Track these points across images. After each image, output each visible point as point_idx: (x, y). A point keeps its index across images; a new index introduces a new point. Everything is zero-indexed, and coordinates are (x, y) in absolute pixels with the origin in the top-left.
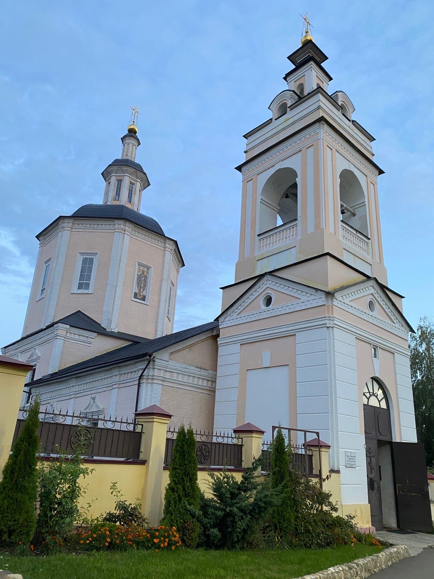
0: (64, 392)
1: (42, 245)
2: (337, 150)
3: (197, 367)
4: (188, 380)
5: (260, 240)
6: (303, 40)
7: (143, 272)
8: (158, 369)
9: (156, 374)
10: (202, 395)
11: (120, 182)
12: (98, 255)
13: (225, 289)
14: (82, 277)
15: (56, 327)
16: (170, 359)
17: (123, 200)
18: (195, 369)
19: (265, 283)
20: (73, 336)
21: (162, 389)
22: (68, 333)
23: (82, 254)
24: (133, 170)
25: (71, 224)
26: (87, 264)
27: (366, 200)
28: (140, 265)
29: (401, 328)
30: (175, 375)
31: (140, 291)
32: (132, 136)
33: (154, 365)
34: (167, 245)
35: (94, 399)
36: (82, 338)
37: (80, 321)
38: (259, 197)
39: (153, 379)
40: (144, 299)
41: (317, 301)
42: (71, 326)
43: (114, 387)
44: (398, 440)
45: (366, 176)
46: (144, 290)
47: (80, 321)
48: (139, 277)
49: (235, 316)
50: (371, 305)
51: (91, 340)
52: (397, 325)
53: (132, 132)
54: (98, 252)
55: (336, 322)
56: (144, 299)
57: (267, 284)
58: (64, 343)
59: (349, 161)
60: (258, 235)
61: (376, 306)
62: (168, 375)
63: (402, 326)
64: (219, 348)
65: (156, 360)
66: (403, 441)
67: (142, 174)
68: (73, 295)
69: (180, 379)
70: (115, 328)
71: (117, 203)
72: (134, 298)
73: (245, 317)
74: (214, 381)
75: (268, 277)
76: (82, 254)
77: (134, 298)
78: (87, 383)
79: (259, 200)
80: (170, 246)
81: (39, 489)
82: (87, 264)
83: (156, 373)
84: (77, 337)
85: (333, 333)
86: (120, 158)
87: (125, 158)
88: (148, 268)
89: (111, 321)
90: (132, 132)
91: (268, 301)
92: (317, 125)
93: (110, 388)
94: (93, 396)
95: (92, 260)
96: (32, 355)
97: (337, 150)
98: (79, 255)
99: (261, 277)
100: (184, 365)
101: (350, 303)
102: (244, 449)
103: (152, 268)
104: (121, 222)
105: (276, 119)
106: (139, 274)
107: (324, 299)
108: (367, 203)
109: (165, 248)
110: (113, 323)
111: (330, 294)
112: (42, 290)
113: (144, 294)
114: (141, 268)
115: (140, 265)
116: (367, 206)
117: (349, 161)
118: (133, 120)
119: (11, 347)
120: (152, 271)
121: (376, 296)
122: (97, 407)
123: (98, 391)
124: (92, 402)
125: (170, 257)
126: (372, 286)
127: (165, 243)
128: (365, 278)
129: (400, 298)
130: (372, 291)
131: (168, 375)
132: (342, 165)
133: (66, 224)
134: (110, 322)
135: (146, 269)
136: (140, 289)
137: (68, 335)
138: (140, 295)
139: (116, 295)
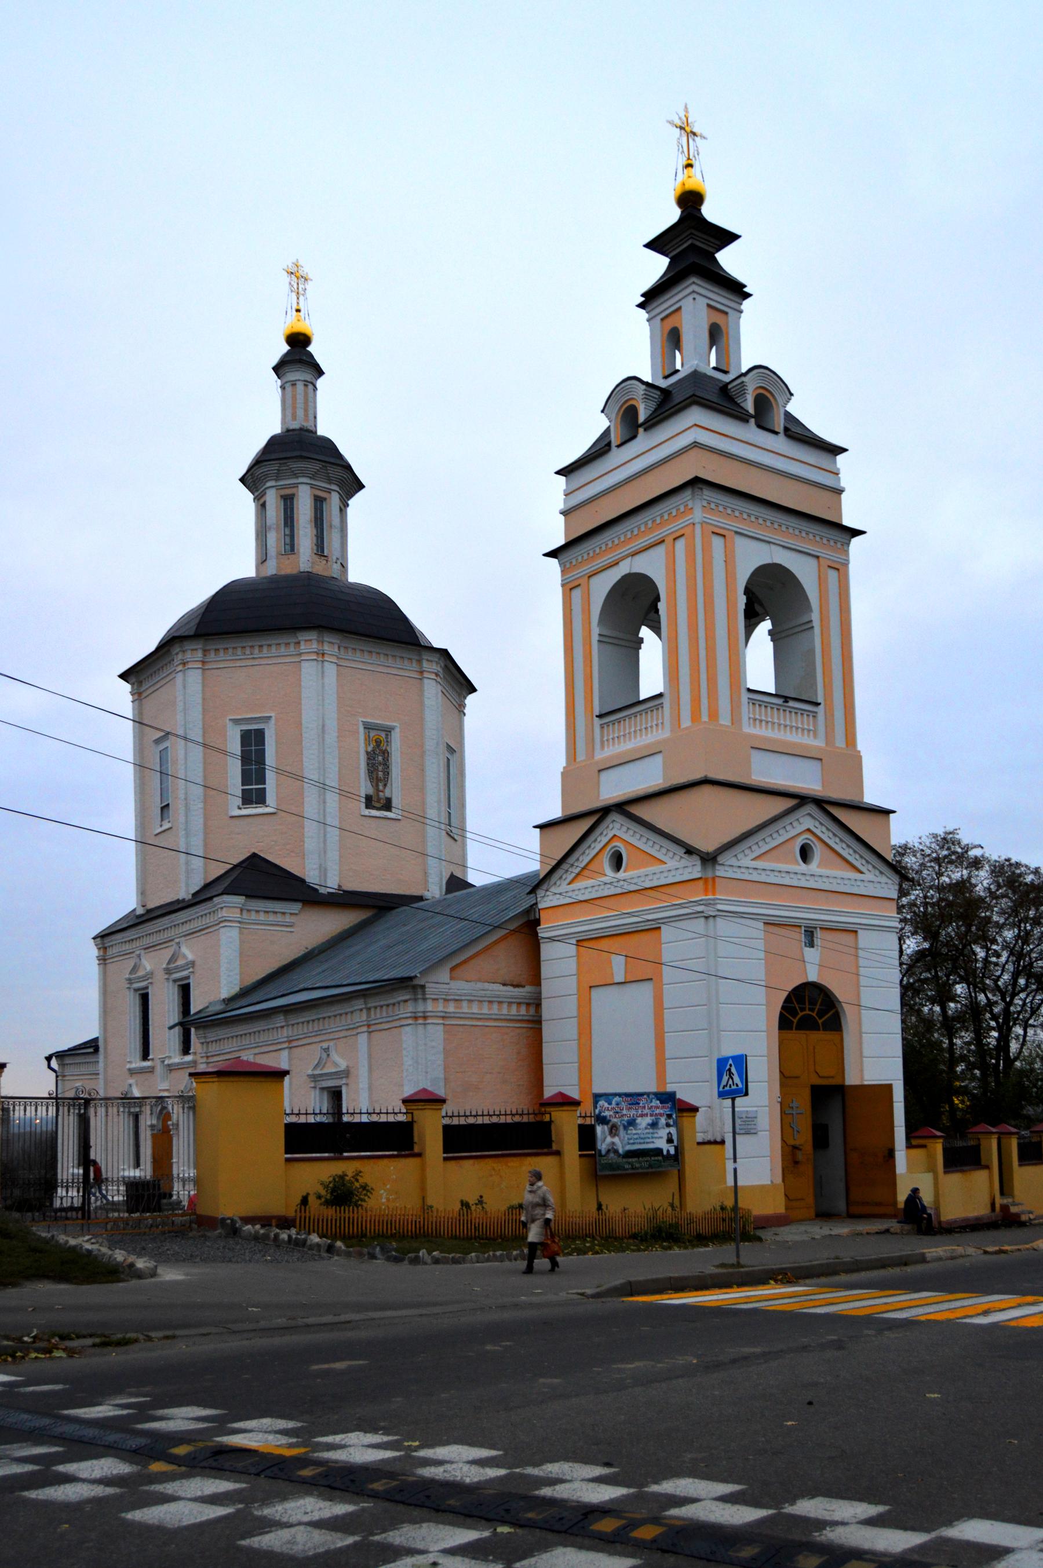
0: (264, 1037)
1: (138, 696)
2: (737, 533)
3: (504, 985)
4: (490, 1009)
5: (602, 726)
6: (679, 191)
7: (378, 743)
8: (434, 999)
9: (430, 1009)
10: (518, 1031)
11: (288, 501)
12: (273, 721)
13: (546, 830)
14: (246, 779)
15: (219, 903)
16: (452, 978)
17: (305, 559)
18: (502, 988)
19: (611, 826)
20: (253, 916)
21: (445, 1032)
22: (245, 912)
23: (236, 721)
24: (317, 466)
25: (199, 654)
26: (253, 743)
27: (815, 616)
28: (368, 727)
29: (879, 879)
30: (465, 1004)
31: (378, 790)
32: (301, 361)
33: (424, 993)
34: (425, 664)
35: (327, 1050)
36: (271, 918)
37: (260, 880)
38: (596, 631)
39: (425, 1018)
40: (387, 806)
41: (690, 870)
42: (247, 896)
43: (359, 1030)
44: (857, 1082)
45: (818, 557)
46: (385, 785)
47: (260, 880)
48: (370, 756)
49: (563, 887)
50: (805, 853)
51: (293, 919)
52: (869, 876)
53: (298, 341)
54: (272, 714)
55: (720, 907)
56: (387, 806)
57: (616, 827)
58: (241, 933)
59: (769, 542)
60: (600, 716)
61: (818, 851)
62: (451, 1008)
63: (881, 873)
64: (543, 947)
65: (427, 985)
66: (866, 1083)
67: (339, 469)
68: (236, 821)
69: (475, 1011)
70: (332, 883)
71: (288, 570)
72: (367, 807)
73: (585, 888)
74: (538, 1005)
75: (615, 816)
76: (236, 721)
77: (367, 807)
78: (308, 1022)
79: (595, 638)
80: (432, 666)
81: (102, 1249)
82: (253, 743)
83: (430, 1006)
84: (262, 917)
85: (715, 926)
86: (277, 430)
87: (295, 425)
88: (388, 731)
89: (326, 869)
90: (298, 341)
91: (617, 861)
92: (687, 493)
93: (355, 1032)
94: (325, 1045)
95: (260, 734)
96: (173, 959)
97: (737, 533)
98: (230, 725)
99: (604, 812)
100: (479, 985)
101: (755, 864)
102: (553, 1127)
103: (397, 730)
104: (313, 635)
105: (618, 446)
106: (370, 749)
107: (699, 868)
108: (816, 624)
109: (422, 672)
110: (329, 875)
111: (709, 859)
112: (162, 808)
113: (387, 794)
114: (372, 734)
115: (368, 727)
116: (817, 630)
117: (769, 542)
118: (295, 306)
119: (119, 936)
120: (396, 735)
121: (818, 832)
122: (336, 1065)
123: (332, 1036)
124: (324, 1055)
125: (433, 691)
126: (809, 814)
127: (420, 661)
128: (790, 803)
129: (880, 818)
130: (808, 823)
131: (451, 1008)
132: (751, 557)
133: (188, 655)
134: (323, 871)
135: (383, 735)
136: (377, 785)
137: (245, 915)
138: (378, 801)
139: (328, 810)
